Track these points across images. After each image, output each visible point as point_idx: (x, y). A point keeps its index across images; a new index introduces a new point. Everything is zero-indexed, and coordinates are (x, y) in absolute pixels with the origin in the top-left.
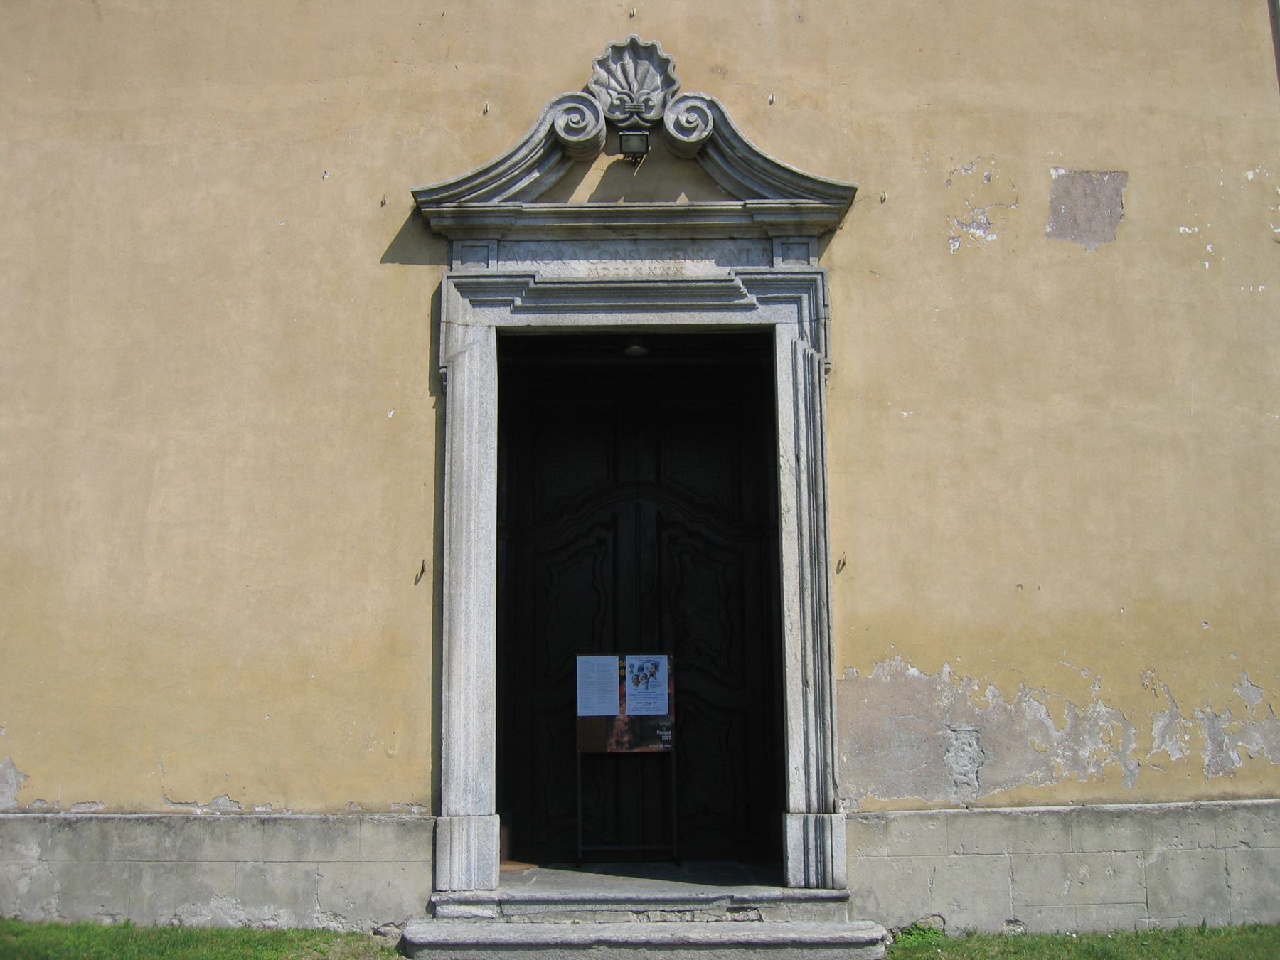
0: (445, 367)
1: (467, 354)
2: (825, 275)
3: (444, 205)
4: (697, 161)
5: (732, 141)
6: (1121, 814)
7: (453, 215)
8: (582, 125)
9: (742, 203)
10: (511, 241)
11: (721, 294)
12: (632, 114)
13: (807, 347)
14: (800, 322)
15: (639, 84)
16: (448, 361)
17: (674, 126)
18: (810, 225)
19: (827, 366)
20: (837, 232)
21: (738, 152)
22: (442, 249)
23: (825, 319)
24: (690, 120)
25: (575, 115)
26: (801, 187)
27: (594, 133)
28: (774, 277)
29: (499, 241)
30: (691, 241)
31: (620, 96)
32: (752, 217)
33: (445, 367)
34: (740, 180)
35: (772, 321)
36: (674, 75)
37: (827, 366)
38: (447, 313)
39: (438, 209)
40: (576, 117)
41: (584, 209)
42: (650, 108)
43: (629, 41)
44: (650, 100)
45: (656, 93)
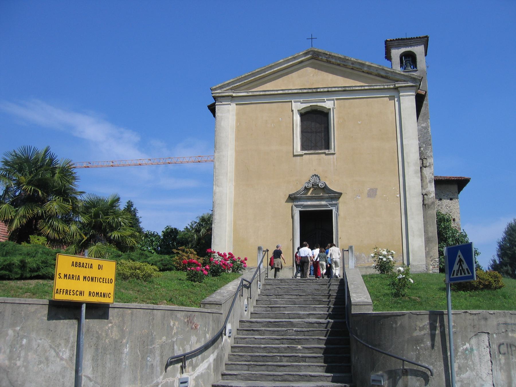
11: (326, 206)
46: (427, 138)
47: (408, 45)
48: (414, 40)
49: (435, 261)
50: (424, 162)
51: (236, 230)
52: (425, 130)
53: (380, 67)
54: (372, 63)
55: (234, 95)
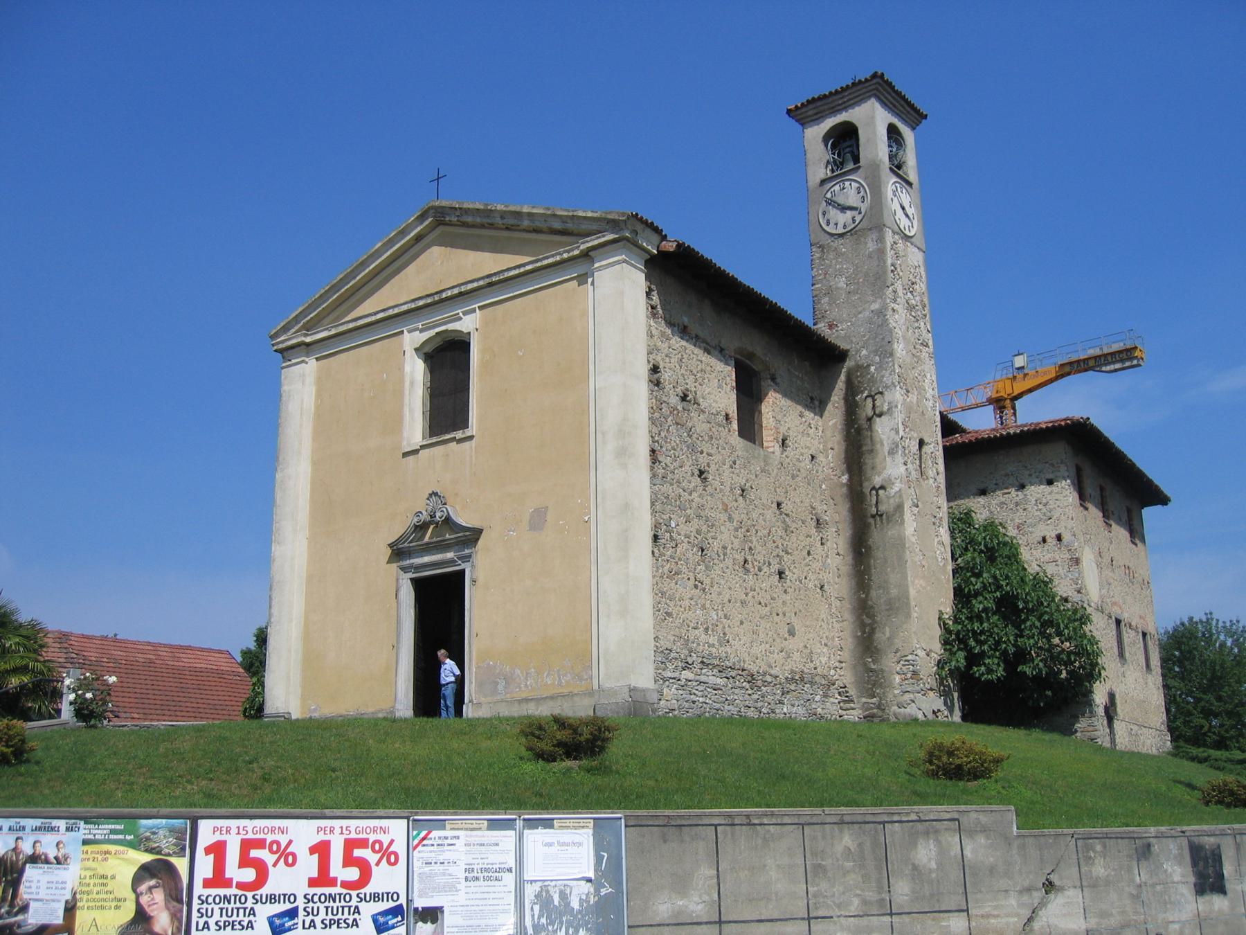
6: (532, 699)
11: (451, 562)
46: (883, 339)
47: (839, 107)
48: (849, 91)
49: (906, 661)
50: (877, 403)
51: (307, 636)
52: (879, 317)
53: (549, 212)
54: (533, 207)
55: (308, 340)
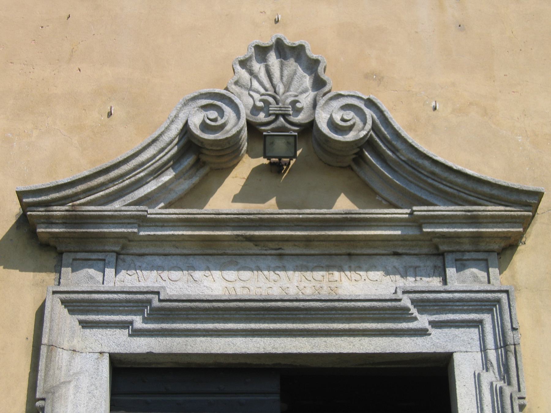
0: (43, 399)
1: (72, 385)
2: (512, 294)
3: (55, 208)
4: (352, 169)
5: (394, 143)
7: (64, 221)
8: (220, 122)
9: (408, 211)
10: (132, 255)
12: (277, 116)
13: (494, 379)
14: (484, 350)
15: (285, 86)
16: (47, 392)
17: (328, 125)
18: (489, 237)
19: (522, 401)
20: (519, 248)
21: (401, 155)
22: (50, 259)
23: (515, 345)
24: (346, 117)
25: (212, 112)
26: (476, 192)
27: (234, 131)
28: (450, 295)
29: (118, 254)
30: (347, 257)
31: (263, 97)
32: (420, 227)
33: (43, 399)
34: (404, 186)
35: (448, 349)
36: (325, 77)
37: (522, 401)
38: (50, 334)
39: (47, 213)
40: (213, 114)
41: (220, 216)
42: (298, 111)
43: (274, 40)
44: (298, 101)
45: (305, 95)
